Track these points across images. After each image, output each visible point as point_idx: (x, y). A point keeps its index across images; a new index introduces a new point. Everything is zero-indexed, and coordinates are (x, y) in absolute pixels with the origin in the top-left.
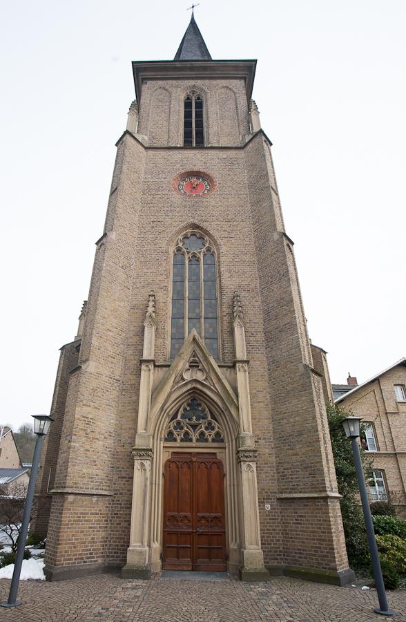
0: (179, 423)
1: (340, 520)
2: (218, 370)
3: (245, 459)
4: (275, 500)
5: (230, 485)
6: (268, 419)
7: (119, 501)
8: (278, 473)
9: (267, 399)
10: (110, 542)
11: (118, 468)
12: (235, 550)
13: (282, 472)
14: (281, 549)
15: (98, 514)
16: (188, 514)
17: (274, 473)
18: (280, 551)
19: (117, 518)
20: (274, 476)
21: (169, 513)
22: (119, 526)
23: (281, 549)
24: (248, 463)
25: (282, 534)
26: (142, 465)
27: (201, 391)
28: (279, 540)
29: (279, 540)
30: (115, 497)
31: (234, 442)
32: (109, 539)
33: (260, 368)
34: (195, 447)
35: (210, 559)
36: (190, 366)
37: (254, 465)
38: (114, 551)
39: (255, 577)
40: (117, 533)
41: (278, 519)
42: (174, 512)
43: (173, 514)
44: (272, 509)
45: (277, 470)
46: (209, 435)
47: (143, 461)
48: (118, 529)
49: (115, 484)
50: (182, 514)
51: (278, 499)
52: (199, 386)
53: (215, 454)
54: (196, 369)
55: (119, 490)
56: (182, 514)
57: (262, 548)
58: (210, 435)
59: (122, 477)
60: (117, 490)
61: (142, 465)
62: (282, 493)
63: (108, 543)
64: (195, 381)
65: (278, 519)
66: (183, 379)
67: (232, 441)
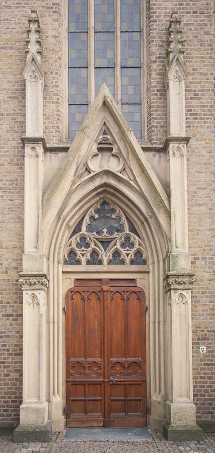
2: (142, 155)
3: (177, 287)
5: (154, 323)
7: (5, 346)
12: (159, 403)
16: (98, 360)
21: (72, 359)
22: (7, 378)
26: (34, 296)
27: (115, 189)
33: (204, 152)
34: (106, 271)
35: (126, 412)
36: (100, 150)
37: (188, 295)
39: (185, 436)
44: (209, 352)
46: (127, 254)
47: (34, 292)
48: (7, 381)
52: (112, 182)
53: (133, 280)
54: (108, 154)
55: (5, 332)
58: (127, 255)
59: (7, 315)
61: (34, 296)
64: (107, 173)
66: (88, 170)
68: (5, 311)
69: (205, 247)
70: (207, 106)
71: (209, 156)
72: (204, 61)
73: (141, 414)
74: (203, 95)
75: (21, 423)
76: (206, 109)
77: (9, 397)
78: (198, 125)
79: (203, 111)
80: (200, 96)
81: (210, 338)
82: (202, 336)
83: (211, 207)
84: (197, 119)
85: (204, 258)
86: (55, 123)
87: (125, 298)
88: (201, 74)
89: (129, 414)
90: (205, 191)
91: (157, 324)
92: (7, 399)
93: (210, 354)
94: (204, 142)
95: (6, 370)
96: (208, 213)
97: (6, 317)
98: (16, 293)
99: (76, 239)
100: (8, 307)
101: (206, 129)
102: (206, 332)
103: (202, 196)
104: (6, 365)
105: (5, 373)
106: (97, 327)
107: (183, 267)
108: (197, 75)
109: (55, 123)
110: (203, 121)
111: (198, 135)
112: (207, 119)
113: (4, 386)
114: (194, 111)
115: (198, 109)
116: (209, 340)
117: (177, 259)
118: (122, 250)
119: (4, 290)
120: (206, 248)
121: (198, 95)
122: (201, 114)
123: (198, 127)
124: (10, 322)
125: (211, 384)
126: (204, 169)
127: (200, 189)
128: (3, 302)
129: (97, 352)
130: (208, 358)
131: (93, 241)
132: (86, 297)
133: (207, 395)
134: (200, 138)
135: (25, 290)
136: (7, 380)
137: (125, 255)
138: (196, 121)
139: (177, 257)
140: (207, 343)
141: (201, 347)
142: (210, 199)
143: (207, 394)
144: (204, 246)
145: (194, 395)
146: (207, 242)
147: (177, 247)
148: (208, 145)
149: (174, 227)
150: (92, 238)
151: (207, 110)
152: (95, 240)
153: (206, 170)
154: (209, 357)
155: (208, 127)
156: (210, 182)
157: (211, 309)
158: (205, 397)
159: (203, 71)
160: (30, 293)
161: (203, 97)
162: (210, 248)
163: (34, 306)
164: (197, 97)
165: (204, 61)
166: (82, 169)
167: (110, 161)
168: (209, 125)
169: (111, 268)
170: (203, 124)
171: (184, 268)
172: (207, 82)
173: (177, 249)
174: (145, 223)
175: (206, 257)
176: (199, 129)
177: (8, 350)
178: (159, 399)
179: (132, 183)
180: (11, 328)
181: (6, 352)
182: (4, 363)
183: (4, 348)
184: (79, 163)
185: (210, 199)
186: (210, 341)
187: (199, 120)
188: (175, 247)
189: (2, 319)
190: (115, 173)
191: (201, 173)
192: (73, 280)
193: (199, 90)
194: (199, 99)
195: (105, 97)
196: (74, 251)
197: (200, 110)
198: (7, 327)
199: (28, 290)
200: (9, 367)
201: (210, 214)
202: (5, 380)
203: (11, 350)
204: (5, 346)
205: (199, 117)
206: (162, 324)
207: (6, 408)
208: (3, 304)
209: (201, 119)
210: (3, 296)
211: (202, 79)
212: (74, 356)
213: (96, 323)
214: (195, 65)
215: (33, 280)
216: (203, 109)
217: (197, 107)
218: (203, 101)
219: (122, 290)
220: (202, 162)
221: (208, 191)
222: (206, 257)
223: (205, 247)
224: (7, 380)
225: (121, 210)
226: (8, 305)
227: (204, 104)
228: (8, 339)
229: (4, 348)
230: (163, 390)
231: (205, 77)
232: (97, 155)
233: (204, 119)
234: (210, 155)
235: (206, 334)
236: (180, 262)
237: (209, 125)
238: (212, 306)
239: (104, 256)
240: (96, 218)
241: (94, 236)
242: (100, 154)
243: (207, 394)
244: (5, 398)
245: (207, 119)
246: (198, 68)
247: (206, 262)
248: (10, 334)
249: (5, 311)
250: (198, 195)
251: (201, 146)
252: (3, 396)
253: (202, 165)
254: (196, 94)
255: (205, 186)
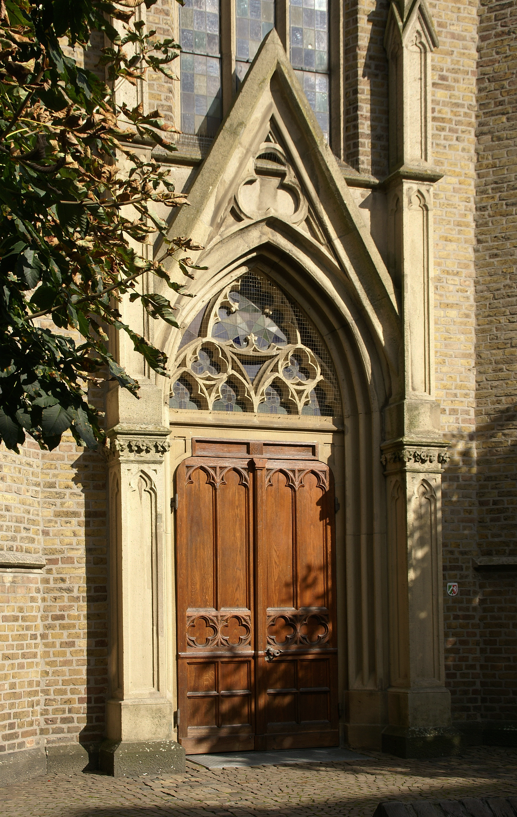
0: (208, 349)
1: (337, 527)
3: (418, 466)
4: (470, 572)
6: (466, 356)
7: (63, 580)
8: (481, 504)
9: (468, 298)
10: (46, 692)
11: (52, 485)
12: (371, 693)
13: (495, 503)
14: (478, 686)
15: (16, 619)
16: (244, 612)
17: (472, 504)
18: (475, 692)
19: (63, 627)
20: (470, 512)
21: (192, 612)
22: (68, 650)
23: (478, 686)
24: (422, 476)
25: (482, 651)
26: (145, 476)
28: (473, 667)
29: (473, 667)
30: (49, 571)
31: (376, 417)
32: (43, 686)
33: (456, 200)
36: (259, 171)
38: (59, 716)
40: (65, 669)
41: (473, 617)
42: (205, 605)
43: (202, 612)
44: (461, 593)
45: (480, 495)
47: (145, 467)
48: (69, 657)
49: (46, 533)
50: (228, 612)
51: (478, 569)
54: (276, 181)
55: (62, 552)
56: (228, 612)
57: (448, 685)
58: (300, 393)
59: (67, 514)
60: (53, 552)
61: (145, 476)
62: (489, 553)
63: (41, 697)
64: (274, 223)
65: (473, 617)
66: (237, 214)
67: (369, 413)
68: (62, 504)
69: (455, 389)
70: (463, 106)
71: (463, 207)
72: (459, 9)
73: (327, 721)
74: (456, 81)
75: (124, 738)
76: (462, 111)
77: (73, 692)
78: (447, 143)
79: (455, 115)
80: (450, 82)
81: (464, 566)
82: (450, 562)
83: (467, 312)
84: (443, 129)
85: (453, 411)
86: (163, 97)
87: (297, 483)
88: (453, 36)
89: (303, 722)
90: (456, 278)
91: (363, 538)
92: (69, 696)
93: (464, 597)
94: (455, 180)
95: (65, 633)
96: (461, 323)
97: (64, 519)
98: (86, 466)
99: (195, 353)
100: (67, 497)
101: (460, 153)
102: (457, 555)
103: (451, 288)
104: (66, 621)
105: (65, 639)
106: (239, 543)
107: (427, 429)
108: (446, 37)
109: (163, 97)
110: (455, 135)
111: (446, 164)
112: (463, 132)
113: (64, 668)
114: (440, 112)
115: (449, 116)
116: (462, 570)
117: (417, 412)
118: (288, 382)
119: (58, 459)
120: (458, 391)
121: (447, 81)
122: (451, 120)
123: (445, 147)
124: (74, 528)
125: (465, 655)
126: (454, 235)
127: (448, 273)
128: (57, 486)
129: (241, 595)
130: (461, 605)
131: (230, 360)
132: (218, 480)
133: (458, 675)
134: (449, 171)
135: (127, 462)
136: (68, 654)
137: (295, 394)
138: (443, 133)
139: (416, 408)
140: (458, 576)
141: (449, 584)
142: (465, 294)
143: (458, 673)
144: (453, 387)
145: (448, 676)
146: (458, 379)
147: (414, 389)
148: (462, 186)
149: (409, 349)
150: (229, 354)
151: (462, 114)
152: (235, 358)
153: (459, 236)
154: (462, 602)
155: (463, 150)
156: (466, 262)
157: (466, 511)
158: (456, 680)
159: (456, 29)
160: (135, 468)
161: (456, 85)
162: (464, 392)
163: (141, 497)
164: (445, 83)
165: (459, 9)
166: (226, 208)
167: (278, 197)
168: (465, 144)
169: (268, 419)
170: (454, 142)
171: (429, 432)
172: (464, 54)
173: (413, 393)
174: (341, 333)
175: (457, 410)
176: (447, 151)
177: (69, 590)
178: (370, 687)
179: (324, 250)
180: (74, 544)
181: (65, 594)
182: (62, 617)
183: (62, 585)
184: (220, 197)
185: (465, 294)
186: (464, 573)
187: (446, 133)
188: (410, 389)
189: (56, 522)
190: (291, 225)
191: (450, 241)
192: (189, 443)
193: (448, 70)
194: (448, 88)
195: (278, 63)
196: (187, 378)
197: (449, 111)
198: (67, 540)
199: (132, 462)
200: (74, 626)
201: (465, 325)
202: (64, 654)
203: (76, 590)
204: (63, 580)
205: (447, 126)
206: (377, 538)
207: (67, 715)
208: (57, 490)
209: (451, 130)
210: (56, 472)
211: (455, 47)
212: (194, 604)
213: (238, 534)
214: (443, 14)
215: (141, 441)
216: (455, 110)
217: (445, 104)
218: (456, 93)
219: (212, 465)
220: (452, 220)
221: (463, 279)
222: (457, 410)
223: (455, 389)
224: (68, 654)
225: (288, 299)
226: (68, 491)
227: (456, 101)
228: (70, 566)
229: (62, 585)
230: (380, 670)
231: (460, 43)
232: (251, 182)
233: (457, 133)
234: (466, 206)
235: (457, 559)
236: (421, 419)
237: (465, 144)
238: (466, 504)
239: (252, 393)
240: (233, 309)
241: (231, 349)
242: (257, 184)
243: (458, 673)
244: (64, 692)
245: (463, 132)
246: (449, 22)
247: (457, 419)
248: (72, 554)
249: (62, 504)
250: (444, 284)
251: (451, 187)
252: (60, 690)
253: (451, 226)
254: (443, 78)
255: (456, 269)
